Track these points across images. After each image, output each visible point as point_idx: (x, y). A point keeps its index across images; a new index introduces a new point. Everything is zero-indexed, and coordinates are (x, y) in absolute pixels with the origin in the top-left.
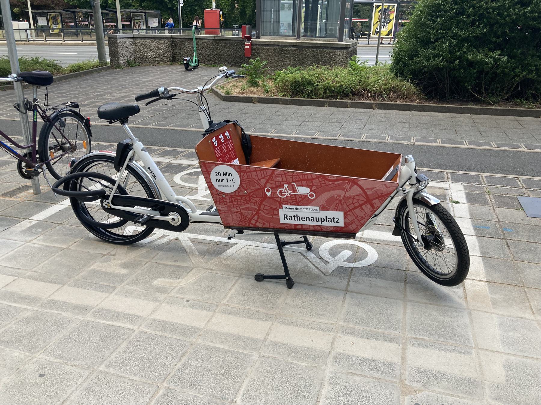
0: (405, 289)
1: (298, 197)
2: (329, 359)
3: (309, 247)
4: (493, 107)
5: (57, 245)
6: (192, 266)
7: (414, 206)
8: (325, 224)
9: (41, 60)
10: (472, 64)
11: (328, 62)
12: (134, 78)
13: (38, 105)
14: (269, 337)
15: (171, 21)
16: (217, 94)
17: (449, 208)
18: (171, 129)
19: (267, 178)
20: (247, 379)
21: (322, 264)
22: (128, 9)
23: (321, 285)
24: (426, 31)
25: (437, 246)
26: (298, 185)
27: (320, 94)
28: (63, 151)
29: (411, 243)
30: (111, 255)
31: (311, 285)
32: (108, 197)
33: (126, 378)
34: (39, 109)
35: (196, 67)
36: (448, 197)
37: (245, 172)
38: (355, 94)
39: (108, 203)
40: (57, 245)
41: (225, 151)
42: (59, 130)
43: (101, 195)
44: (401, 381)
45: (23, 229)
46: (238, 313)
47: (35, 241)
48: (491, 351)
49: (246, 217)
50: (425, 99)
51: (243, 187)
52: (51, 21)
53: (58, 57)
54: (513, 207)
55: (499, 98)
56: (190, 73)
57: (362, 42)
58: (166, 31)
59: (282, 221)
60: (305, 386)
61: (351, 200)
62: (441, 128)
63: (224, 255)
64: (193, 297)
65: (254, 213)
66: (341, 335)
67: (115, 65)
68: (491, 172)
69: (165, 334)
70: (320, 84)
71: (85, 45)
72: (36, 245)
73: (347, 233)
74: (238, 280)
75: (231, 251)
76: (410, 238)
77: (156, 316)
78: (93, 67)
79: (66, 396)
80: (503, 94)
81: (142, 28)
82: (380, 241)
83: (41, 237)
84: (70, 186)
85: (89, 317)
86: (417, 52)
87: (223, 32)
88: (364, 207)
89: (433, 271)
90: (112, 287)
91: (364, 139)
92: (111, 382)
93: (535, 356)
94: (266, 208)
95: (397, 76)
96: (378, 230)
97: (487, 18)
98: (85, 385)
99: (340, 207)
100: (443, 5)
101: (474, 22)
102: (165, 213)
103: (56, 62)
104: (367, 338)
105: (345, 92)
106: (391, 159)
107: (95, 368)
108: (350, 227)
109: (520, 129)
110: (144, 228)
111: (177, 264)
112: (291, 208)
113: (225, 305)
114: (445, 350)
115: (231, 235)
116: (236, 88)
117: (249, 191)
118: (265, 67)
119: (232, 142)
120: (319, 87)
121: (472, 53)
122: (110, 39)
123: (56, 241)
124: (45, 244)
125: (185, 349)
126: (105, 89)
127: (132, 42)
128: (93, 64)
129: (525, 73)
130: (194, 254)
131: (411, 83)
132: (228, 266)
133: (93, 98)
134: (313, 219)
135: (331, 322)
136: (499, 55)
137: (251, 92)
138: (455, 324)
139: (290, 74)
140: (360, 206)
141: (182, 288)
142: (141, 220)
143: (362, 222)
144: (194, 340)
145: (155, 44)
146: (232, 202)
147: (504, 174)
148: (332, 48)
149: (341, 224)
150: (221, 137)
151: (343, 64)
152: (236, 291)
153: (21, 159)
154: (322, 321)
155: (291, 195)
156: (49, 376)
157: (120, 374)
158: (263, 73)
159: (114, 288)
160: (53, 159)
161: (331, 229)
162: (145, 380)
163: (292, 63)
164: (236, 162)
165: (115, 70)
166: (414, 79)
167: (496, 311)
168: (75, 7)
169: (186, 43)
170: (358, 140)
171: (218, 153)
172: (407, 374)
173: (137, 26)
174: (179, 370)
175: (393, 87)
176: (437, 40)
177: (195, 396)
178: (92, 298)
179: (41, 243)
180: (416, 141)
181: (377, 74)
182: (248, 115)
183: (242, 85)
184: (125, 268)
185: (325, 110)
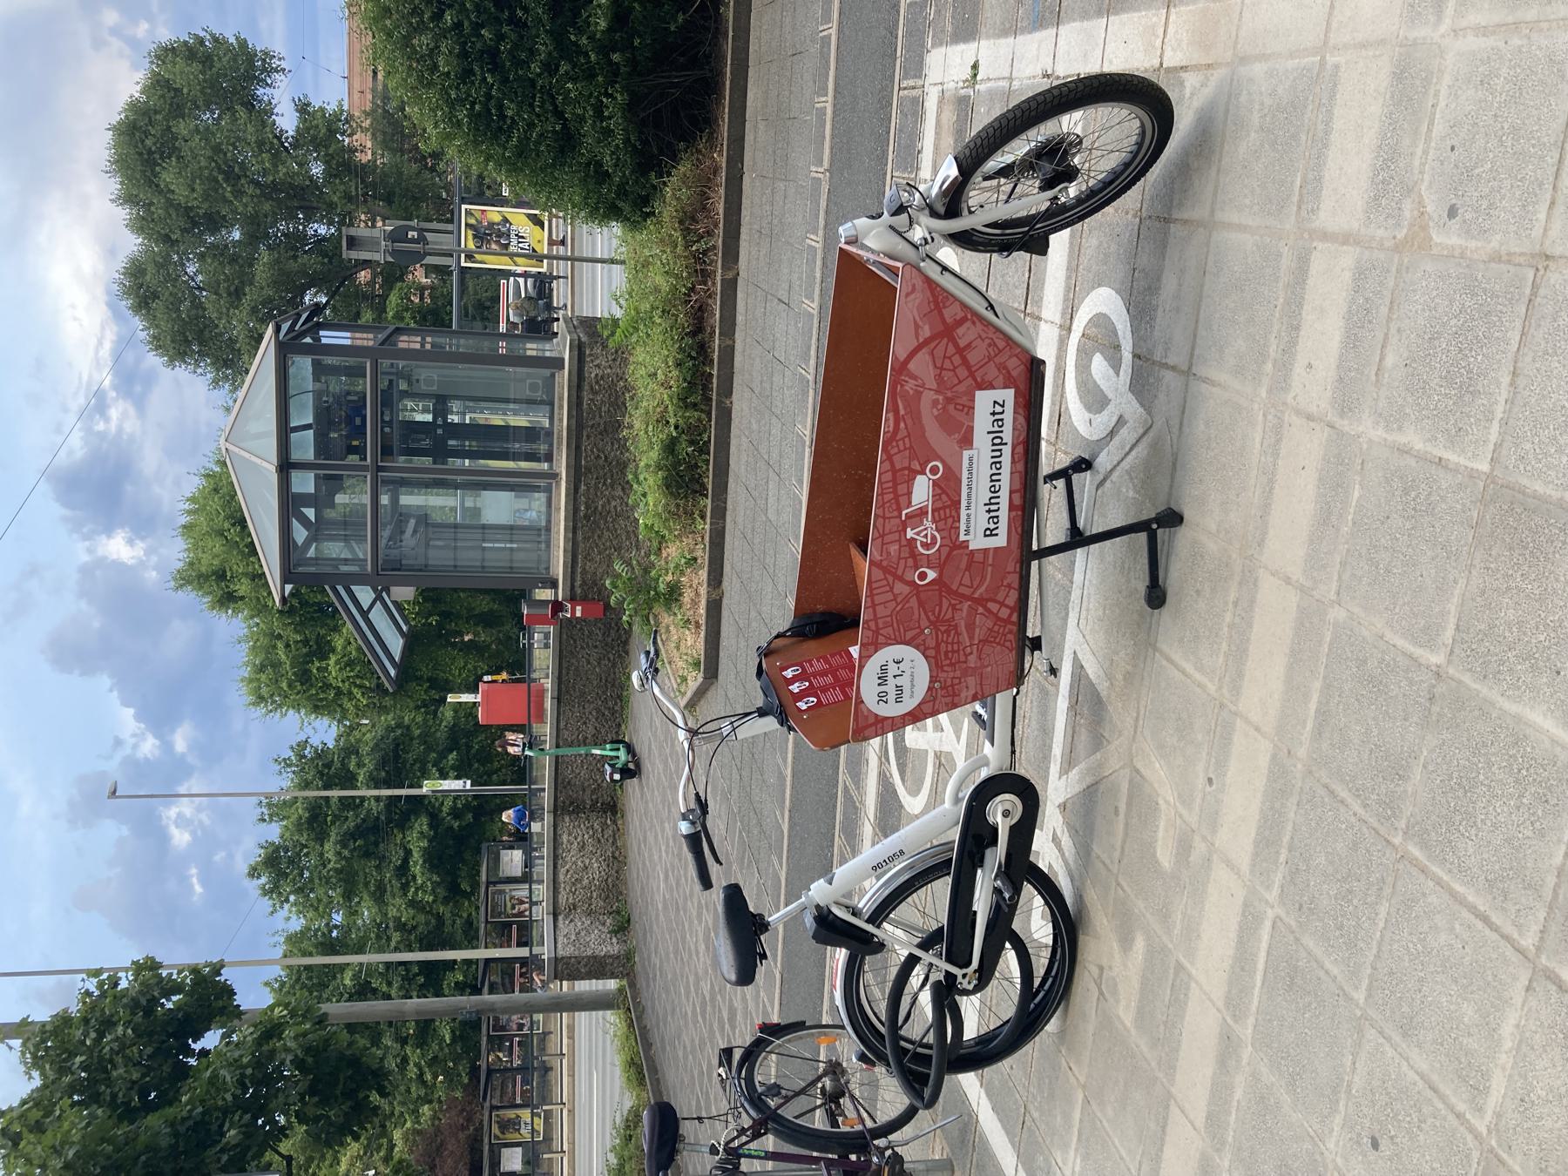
0: (1186, 222)
1: (939, 504)
2: (1347, 429)
5: (1077, 1115)
6: (1127, 770)
7: (965, 212)
8: (1007, 435)
9: (614, 1161)
11: (617, 397)
13: (727, 1144)
14: (1294, 578)
15: (508, 816)
16: (700, 693)
18: (790, 818)
19: (891, 579)
20: (1389, 635)
21: (1124, 432)
22: (477, 930)
23: (1175, 437)
24: (538, 143)
25: (1066, 152)
26: (909, 504)
27: (699, 420)
29: (1065, 208)
30: (1101, 976)
31: (1174, 464)
33: (1382, 936)
34: (736, 1143)
35: (630, 749)
36: (963, 92)
37: (877, 632)
39: (964, 976)
40: (1077, 1115)
41: (829, 679)
42: (787, 1099)
43: (946, 994)
44: (1398, 248)
46: (1239, 653)
48: (1330, 14)
49: (991, 630)
51: (914, 638)
52: (512, 1137)
53: (604, 1119)
56: (647, 766)
58: (536, 827)
59: (1001, 541)
60: (1406, 492)
61: (947, 375)
63: (1103, 687)
65: (981, 610)
66: (1292, 394)
67: (623, 965)
69: (1286, 839)
70: (672, 421)
71: (572, 1047)
72: (1077, 1169)
74: (1162, 653)
75: (1092, 669)
76: (1047, 215)
77: (1244, 862)
78: (631, 1025)
79: (1421, 1084)
81: (526, 893)
82: (1068, 278)
84: (925, 1070)
85: (1246, 1031)
86: (588, 164)
87: (534, 676)
88: (962, 343)
89: (1135, 155)
90: (1176, 974)
91: (815, 305)
92: (1391, 973)
94: (966, 581)
98: (1397, 1038)
99: (964, 400)
100: (473, 104)
101: (514, 21)
102: (991, 836)
103: (618, 1120)
104: (1297, 328)
105: (694, 354)
106: (852, 276)
107: (1359, 1013)
108: (1014, 373)
110: (1028, 889)
111: (1122, 807)
112: (968, 521)
113: (1220, 688)
114: (1327, 133)
115: (1046, 668)
116: (682, 642)
117: (924, 623)
118: (629, 564)
119: (810, 661)
121: (592, 20)
122: (558, 976)
123: (1067, 1117)
124: (1073, 1146)
125: (1321, 792)
126: (688, 993)
127: (566, 917)
130: (1100, 766)
131: (669, 174)
132: (1128, 677)
133: (711, 1026)
134: (996, 464)
135: (1261, 417)
137: (695, 603)
138: (1268, 101)
139: (648, 499)
140: (960, 351)
141: (1180, 796)
142: (1007, 896)
143: (1001, 344)
144: (1299, 766)
145: (571, 857)
146: (952, 664)
148: (579, 387)
149: (1008, 395)
150: (795, 688)
151: (621, 356)
152: (1186, 656)
154: (1258, 440)
155: (934, 521)
156: (1376, 1127)
157: (1374, 951)
158: (646, 571)
159: (1179, 967)
160: (862, 1121)
161: (1021, 419)
162: (1387, 891)
164: (855, 651)
165: (638, 968)
168: (474, 1071)
169: (568, 773)
170: (816, 321)
171: (835, 695)
172: (1380, 233)
173: (523, 907)
174: (1365, 806)
175: (681, 222)
176: (559, 115)
177: (1425, 767)
178: (1201, 1024)
179: (1072, 1153)
180: (821, 165)
181: (646, 265)
182: (753, 614)
183: (676, 626)
184: (1133, 940)
185: (740, 404)
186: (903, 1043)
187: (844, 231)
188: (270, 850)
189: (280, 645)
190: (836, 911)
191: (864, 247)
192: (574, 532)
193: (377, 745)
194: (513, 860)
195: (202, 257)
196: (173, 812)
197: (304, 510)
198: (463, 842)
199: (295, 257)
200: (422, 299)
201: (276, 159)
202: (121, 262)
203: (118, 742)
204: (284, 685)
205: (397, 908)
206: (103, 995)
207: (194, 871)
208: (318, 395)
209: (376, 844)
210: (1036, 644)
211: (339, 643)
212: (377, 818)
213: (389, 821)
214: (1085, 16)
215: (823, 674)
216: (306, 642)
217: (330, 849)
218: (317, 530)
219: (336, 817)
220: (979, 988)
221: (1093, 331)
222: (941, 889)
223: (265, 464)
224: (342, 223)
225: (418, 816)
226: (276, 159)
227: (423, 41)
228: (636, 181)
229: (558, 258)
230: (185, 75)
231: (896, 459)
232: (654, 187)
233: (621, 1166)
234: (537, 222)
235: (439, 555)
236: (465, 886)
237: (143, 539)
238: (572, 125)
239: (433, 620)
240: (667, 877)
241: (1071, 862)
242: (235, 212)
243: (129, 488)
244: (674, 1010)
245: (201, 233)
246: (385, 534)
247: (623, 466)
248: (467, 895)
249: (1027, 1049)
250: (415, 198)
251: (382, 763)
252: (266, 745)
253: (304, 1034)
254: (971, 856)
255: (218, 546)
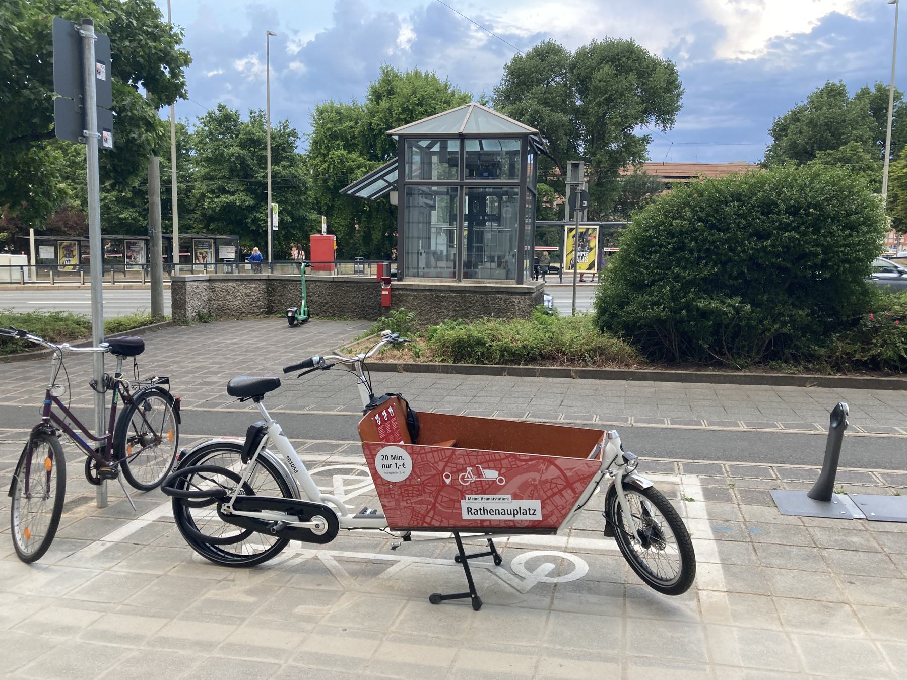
1: (484, 484)
3: (498, 561)
4: (742, 374)
5: (149, 572)
8: (519, 517)
9: (65, 315)
10: (704, 314)
11: (504, 313)
12: (209, 339)
15: (256, 251)
17: (680, 508)
19: (446, 460)
21: (517, 580)
25: (656, 541)
26: (484, 468)
28: (144, 445)
29: (628, 543)
32: (229, 499)
36: (679, 494)
37: (419, 454)
38: (545, 357)
39: (229, 507)
40: (149, 572)
41: (389, 431)
42: (143, 415)
43: (218, 497)
45: (95, 553)
47: (116, 568)
50: (646, 363)
52: (61, 253)
54: (764, 504)
55: (749, 360)
56: (296, 331)
57: (552, 279)
59: (465, 516)
62: (670, 403)
63: (383, 575)
64: (350, 625)
67: (180, 318)
68: (737, 460)
69: (321, 667)
70: (494, 344)
72: (119, 573)
73: (546, 528)
75: (392, 570)
76: (625, 534)
80: (753, 355)
82: (591, 550)
83: (124, 563)
84: (177, 487)
85: (216, 654)
86: (628, 298)
90: (239, 618)
91: (562, 420)
93: (781, 669)
94: (445, 499)
95: (603, 332)
96: (587, 537)
97: (717, 254)
99: (536, 494)
100: (656, 238)
101: (700, 258)
102: (304, 518)
104: (579, 659)
108: (549, 520)
109: (778, 403)
110: (273, 540)
111: (323, 588)
112: (476, 499)
115: (396, 544)
117: (423, 478)
118: (412, 320)
120: (494, 348)
126: (169, 357)
127: (208, 287)
128: (140, 319)
129: (776, 326)
130: (342, 576)
132: (391, 588)
134: (505, 512)
136: (740, 302)
137: (394, 357)
138: (686, 640)
139: (452, 331)
140: (560, 491)
143: (563, 512)
145: (242, 289)
146: (401, 493)
147: (753, 462)
148: (508, 293)
149: (538, 517)
150: (384, 413)
151: (526, 315)
152: (410, 615)
153: (92, 454)
155: (476, 481)
161: (526, 524)
163: (451, 314)
164: (402, 443)
165: (179, 328)
166: (628, 335)
167: (737, 624)
169: (290, 287)
173: (201, 259)
175: (599, 347)
176: (653, 283)
178: (216, 631)
181: (574, 328)
185: (505, 381)
186: (190, 476)
187: (614, 432)
188: (234, 117)
189: (352, 123)
190: (266, 437)
191: (606, 445)
192: (429, 290)
193: (296, 177)
194: (229, 253)
195: (565, 85)
196: (255, 61)
197: (438, 144)
198: (240, 226)
199: (566, 134)
200: (545, 202)
201: (617, 124)
202: (559, 42)
203: (296, 32)
204: (329, 126)
205: (200, 187)
206: (171, 36)
207: (221, 72)
208: (498, 153)
209: (238, 176)
210: (407, 538)
211: (354, 155)
212: (253, 177)
213: (251, 184)
214: (721, 552)
215: (391, 427)
216: (354, 137)
217: (236, 150)
218: (427, 153)
219: (254, 153)
220: (221, 515)
221: (566, 563)
222: (277, 494)
223: (463, 127)
224: (585, 159)
225: (254, 199)
226: (617, 124)
227: (688, 212)
228: (619, 323)
229: (575, 278)
230: (659, 79)
231: (506, 461)
232: (616, 333)
233: (62, 320)
234: (591, 267)
235: (414, 215)
236: (212, 226)
237: (411, 48)
238: (648, 289)
239: (367, 208)
240: (235, 344)
241: (288, 563)
242: (590, 102)
243: (439, 41)
244: (157, 349)
245: (578, 85)
246: (425, 189)
247: (465, 316)
248: (207, 226)
249: (184, 542)
250: (599, 198)
251: (285, 180)
252: (297, 118)
253: (149, 144)
254: (292, 509)
255: (407, 91)
